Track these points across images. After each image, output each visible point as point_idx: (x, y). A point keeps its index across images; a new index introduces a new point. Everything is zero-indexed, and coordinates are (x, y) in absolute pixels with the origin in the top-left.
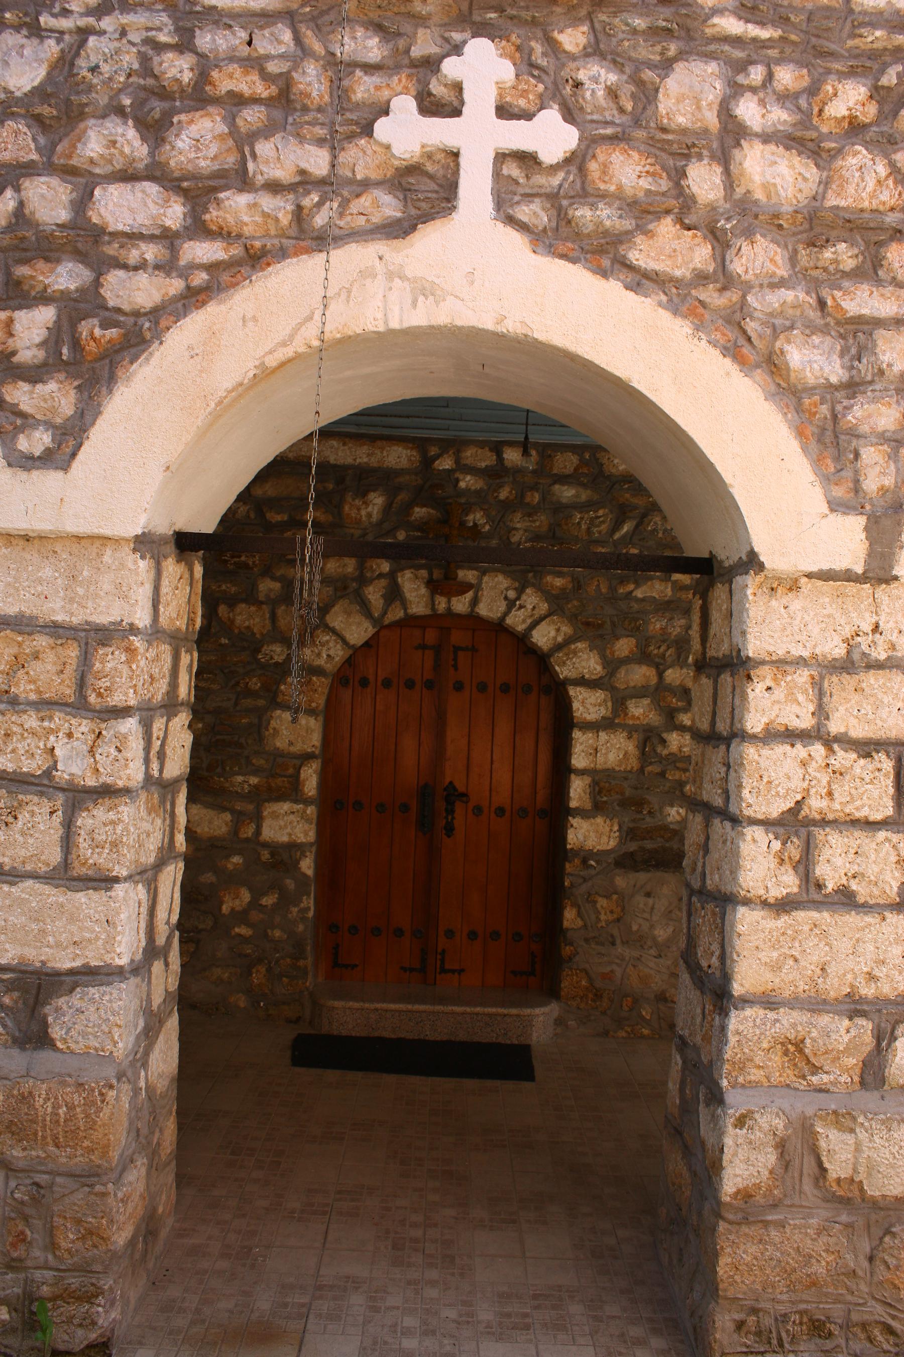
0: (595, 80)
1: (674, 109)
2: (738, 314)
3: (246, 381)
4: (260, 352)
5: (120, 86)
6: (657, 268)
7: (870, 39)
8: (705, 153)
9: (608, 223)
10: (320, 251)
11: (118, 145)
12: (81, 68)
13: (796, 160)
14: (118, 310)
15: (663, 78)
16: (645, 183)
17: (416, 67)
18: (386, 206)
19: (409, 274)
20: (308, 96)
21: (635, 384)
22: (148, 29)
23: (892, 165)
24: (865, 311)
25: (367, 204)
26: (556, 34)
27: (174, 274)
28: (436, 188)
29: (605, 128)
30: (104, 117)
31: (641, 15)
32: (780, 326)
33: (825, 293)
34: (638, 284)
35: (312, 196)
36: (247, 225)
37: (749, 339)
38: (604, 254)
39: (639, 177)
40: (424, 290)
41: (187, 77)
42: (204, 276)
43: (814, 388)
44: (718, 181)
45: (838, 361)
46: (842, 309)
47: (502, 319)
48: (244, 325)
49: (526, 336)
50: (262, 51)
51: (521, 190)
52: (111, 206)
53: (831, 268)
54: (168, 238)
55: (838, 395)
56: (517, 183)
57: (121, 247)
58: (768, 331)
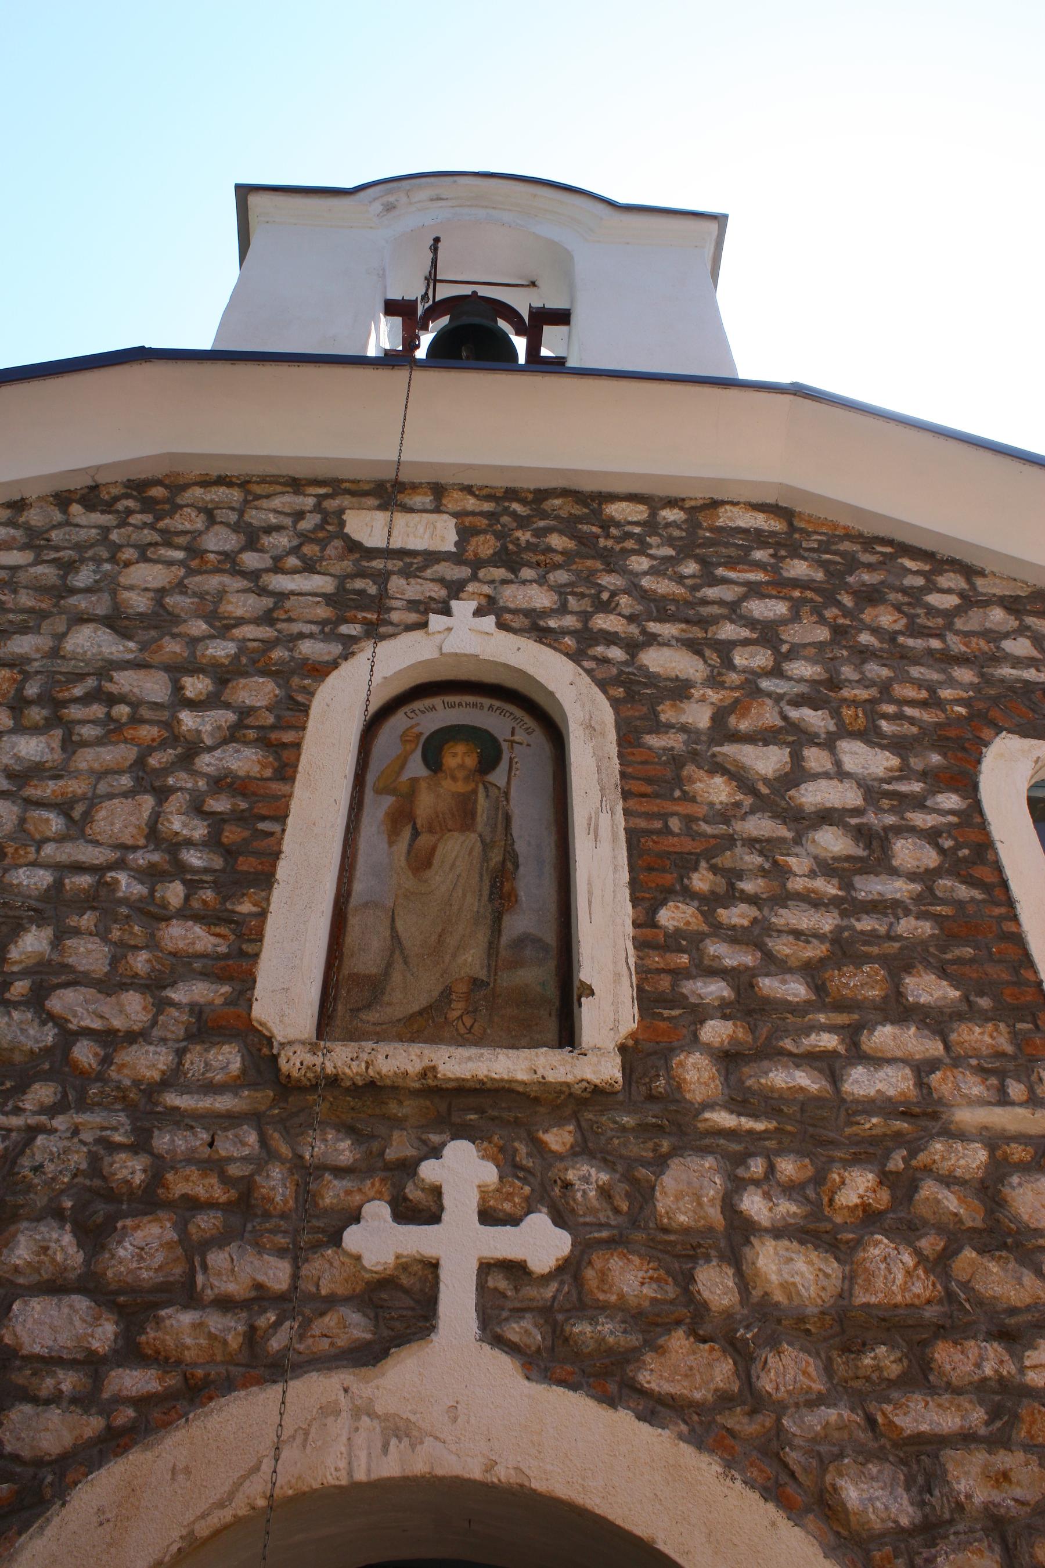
0: (586, 1179)
1: (674, 1207)
2: (775, 1442)
3: (167, 1559)
4: (190, 1516)
5: (63, 1187)
6: (672, 1390)
7: (867, 1126)
8: (713, 1253)
9: (611, 1340)
10: (275, 1382)
11: (50, 1252)
12: (23, 1167)
13: (814, 1255)
14: (16, 1458)
15: (659, 1174)
16: (649, 1291)
17: (391, 1170)
18: (354, 1326)
19: (379, 1409)
20: (271, 1201)
21: (660, 1546)
22: (103, 1128)
23: (918, 1253)
24: (924, 1427)
25: (332, 1324)
26: (540, 1134)
27: (93, 1410)
28: (412, 1303)
29: (600, 1231)
30: (39, 1219)
31: (629, 1113)
32: (827, 1454)
33: (872, 1407)
34: (653, 1412)
35: (269, 1315)
36: (188, 1348)
37: (792, 1474)
38: (608, 1378)
39: (642, 1284)
40: (398, 1430)
41: (138, 1178)
42: (131, 1413)
43: (882, 1535)
44: (731, 1284)
45: (905, 1496)
46: (896, 1426)
47: (490, 1466)
48: (173, 1479)
49: (522, 1486)
50: (223, 1153)
51: (510, 1305)
52: (29, 1324)
53: (875, 1376)
54: (93, 1364)
55: (915, 1542)
56: (505, 1296)
57: (34, 1374)
58: (814, 1463)
